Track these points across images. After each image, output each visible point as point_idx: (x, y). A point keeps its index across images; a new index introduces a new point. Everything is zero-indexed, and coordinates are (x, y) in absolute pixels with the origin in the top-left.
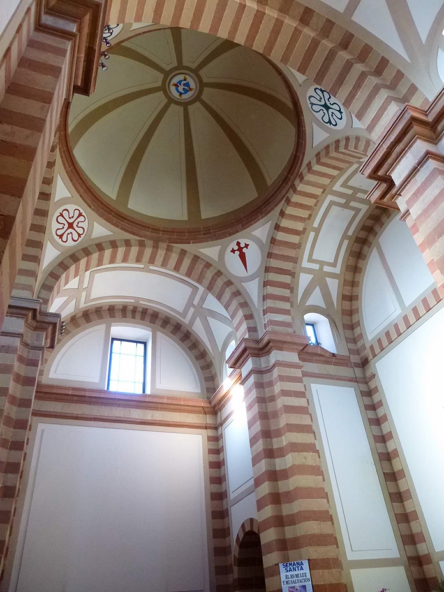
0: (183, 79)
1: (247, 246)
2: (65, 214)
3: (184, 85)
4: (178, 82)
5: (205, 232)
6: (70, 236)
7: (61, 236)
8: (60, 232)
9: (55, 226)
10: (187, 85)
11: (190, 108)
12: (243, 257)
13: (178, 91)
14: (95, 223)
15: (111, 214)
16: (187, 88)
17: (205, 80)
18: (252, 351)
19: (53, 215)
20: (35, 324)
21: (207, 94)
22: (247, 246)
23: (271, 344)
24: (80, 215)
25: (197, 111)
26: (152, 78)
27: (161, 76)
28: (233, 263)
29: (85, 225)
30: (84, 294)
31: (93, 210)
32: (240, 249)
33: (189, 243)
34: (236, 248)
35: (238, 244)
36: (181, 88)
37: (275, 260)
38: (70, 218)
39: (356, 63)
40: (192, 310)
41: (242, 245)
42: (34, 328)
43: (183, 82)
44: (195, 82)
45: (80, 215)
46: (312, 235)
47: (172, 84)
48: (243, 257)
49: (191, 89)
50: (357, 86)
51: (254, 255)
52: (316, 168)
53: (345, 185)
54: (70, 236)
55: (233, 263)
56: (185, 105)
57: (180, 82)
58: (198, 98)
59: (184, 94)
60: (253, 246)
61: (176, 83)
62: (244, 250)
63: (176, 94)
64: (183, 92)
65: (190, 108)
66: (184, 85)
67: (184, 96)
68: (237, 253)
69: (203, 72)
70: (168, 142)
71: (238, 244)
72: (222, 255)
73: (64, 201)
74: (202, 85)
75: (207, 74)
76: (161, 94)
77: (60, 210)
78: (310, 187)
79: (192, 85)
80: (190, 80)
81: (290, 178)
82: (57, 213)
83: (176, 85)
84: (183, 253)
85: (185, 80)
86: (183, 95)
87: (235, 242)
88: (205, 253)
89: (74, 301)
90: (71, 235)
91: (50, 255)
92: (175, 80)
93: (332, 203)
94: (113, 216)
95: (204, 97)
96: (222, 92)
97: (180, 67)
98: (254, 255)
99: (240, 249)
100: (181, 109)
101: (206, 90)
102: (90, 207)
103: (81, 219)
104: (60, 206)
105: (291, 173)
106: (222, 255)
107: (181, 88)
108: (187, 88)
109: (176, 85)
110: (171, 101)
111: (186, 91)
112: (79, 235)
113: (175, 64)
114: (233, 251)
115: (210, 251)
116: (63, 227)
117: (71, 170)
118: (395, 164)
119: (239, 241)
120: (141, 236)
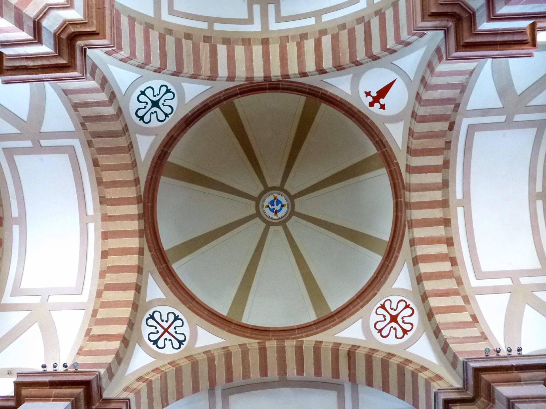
0: (268, 208)
1: (368, 94)
2: (380, 326)
3: (273, 206)
4: (273, 212)
5: (382, 146)
6: (407, 320)
7: (405, 332)
8: (400, 333)
9: (391, 341)
10: (272, 203)
11: (293, 193)
12: (383, 93)
13: (281, 209)
14: (395, 286)
15: (388, 265)
16: (275, 202)
17: (261, 188)
18: (466, 33)
19: (379, 343)
20: (482, 399)
21: (274, 181)
22: (368, 94)
23: (434, 10)
24: (383, 307)
25: (295, 184)
26: (276, 235)
27: (272, 228)
28: (398, 100)
29: (395, 299)
30: (524, 281)
31: (378, 291)
32: (376, 100)
33: (397, 163)
34: (377, 105)
35: (371, 104)
36: (277, 208)
37: (358, 54)
38: (385, 320)
39: (106, 94)
40: (518, 118)
41: (370, 99)
42: (490, 401)
43: (271, 207)
44: (267, 197)
45: (383, 307)
46: (326, 18)
47: (275, 217)
48: (383, 93)
49: (275, 199)
50: (86, 105)
51: (373, 80)
52: (223, 72)
53: (250, 21)
54: (407, 320)
55: (398, 100)
56: (292, 198)
57: (272, 210)
58: (281, 188)
59: (281, 203)
60: (363, 87)
61: (274, 214)
62: (374, 94)
63: (285, 209)
64: (280, 205)
65: (293, 193)
66: (273, 206)
67: (284, 202)
68: (382, 101)
69: (256, 194)
70: (327, 205)
71: (371, 104)
72: (394, 119)
73: (366, 329)
74: (267, 190)
75: (255, 189)
76: (289, 224)
77: (375, 332)
78: (254, 63)
79: (271, 198)
80: (267, 202)
81: (269, 85)
82: (378, 336)
83: (276, 212)
84: (410, 169)
85: (268, 206)
86: (283, 203)
87: (371, 108)
88: (401, 140)
89: (537, 294)
90: (405, 319)
91: (423, 350)
92: (272, 215)
93: (279, 19)
94: (389, 263)
95: (277, 183)
96: (265, 173)
97: (258, 214)
98: (373, 80)
99: (376, 100)
100: (297, 201)
101: (270, 185)
102: (376, 294)
103: (387, 305)
104: (370, 332)
105: (207, 106)
106: (394, 119)
107: (277, 208)
108: (275, 202)
109: (276, 212)
110: (292, 213)
111: (278, 202)
112: (407, 306)
113: (257, 220)
114: (383, 107)
115: (396, 134)
116: (395, 329)
117: (338, 318)
118: (60, 30)
119: (367, 105)
120: (405, 225)
